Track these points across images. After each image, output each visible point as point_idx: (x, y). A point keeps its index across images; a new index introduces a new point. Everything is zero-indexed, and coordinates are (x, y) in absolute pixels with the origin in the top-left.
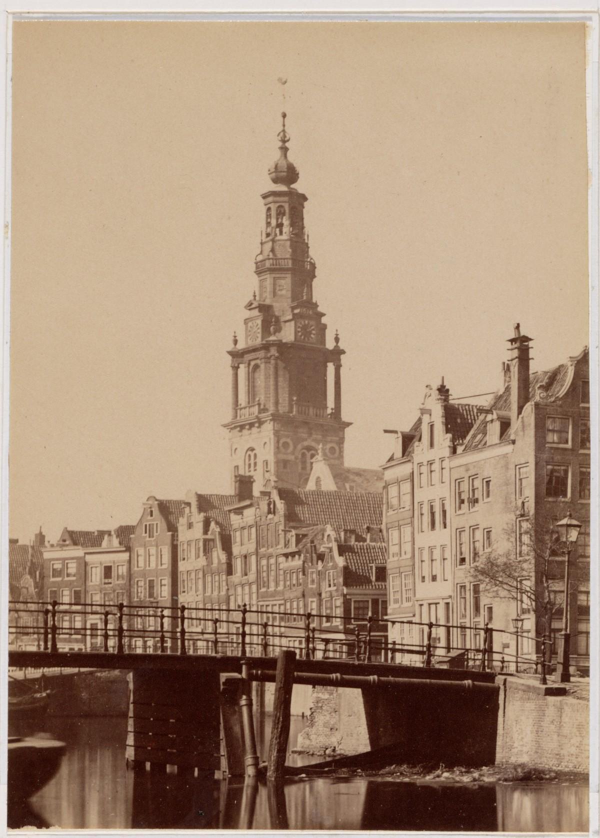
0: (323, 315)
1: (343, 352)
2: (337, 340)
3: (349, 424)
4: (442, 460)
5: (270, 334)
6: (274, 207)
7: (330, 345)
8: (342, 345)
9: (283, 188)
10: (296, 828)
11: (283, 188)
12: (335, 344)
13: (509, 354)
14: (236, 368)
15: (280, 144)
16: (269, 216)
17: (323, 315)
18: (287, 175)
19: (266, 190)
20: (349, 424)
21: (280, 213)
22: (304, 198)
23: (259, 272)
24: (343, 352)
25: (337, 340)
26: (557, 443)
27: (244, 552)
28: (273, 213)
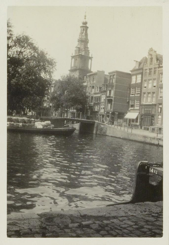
1: (93, 58)
2: (92, 55)
3: (69, 70)
4: (155, 68)
5: (80, 52)
6: (82, 29)
8: (93, 56)
9: (84, 25)
10: (8, 217)
11: (84, 25)
13: (77, 33)
14: (72, 59)
15: (86, 17)
16: (81, 30)
18: (85, 23)
19: (81, 26)
20: (69, 70)
21: (84, 30)
22: (88, 27)
23: (78, 41)
24: (93, 58)
25: (92, 55)
26: (143, 71)
27: (150, 67)
28: (82, 30)
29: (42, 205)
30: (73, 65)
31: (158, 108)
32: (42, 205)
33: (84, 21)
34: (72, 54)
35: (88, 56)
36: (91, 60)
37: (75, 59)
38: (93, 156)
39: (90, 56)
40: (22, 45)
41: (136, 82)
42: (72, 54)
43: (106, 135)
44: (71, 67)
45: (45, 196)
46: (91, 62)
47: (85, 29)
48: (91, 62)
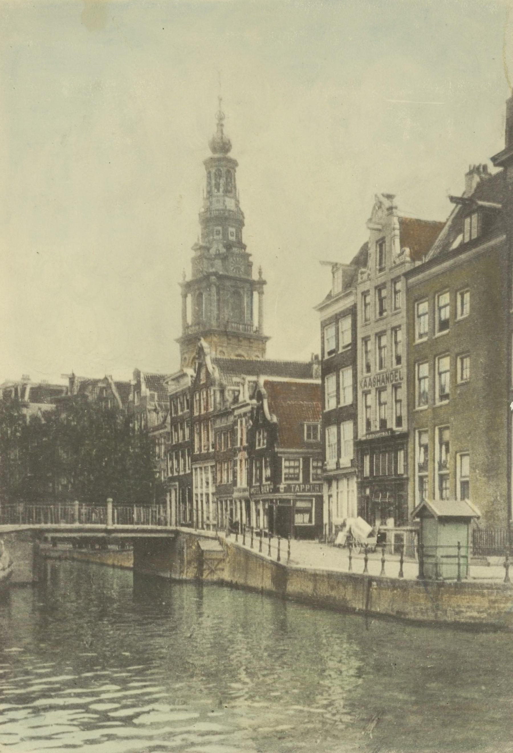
0: (250, 255)
2: (260, 273)
6: (213, 171)
7: (255, 277)
8: (264, 277)
12: (258, 276)
16: (209, 177)
17: (250, 255)
25: (260, 273)
28: (213, 176)
29: (5, 745)
30: (190, 320)
31: (437, 376)
32: (5, 745)
33: (177, 341)
34: (185, 277)
35: (250, 278)
36: (261, 293)
37: (197, 292)
38: (468, 370)
39: (255, 277)
40: (19, 555)
41: (337, 407)
42: (185, 277)
43: (247, 573)
44: (186, 327)
45: (80, 746)
46: (260, 301)
47: (224, 170)
48: (260, 301)
